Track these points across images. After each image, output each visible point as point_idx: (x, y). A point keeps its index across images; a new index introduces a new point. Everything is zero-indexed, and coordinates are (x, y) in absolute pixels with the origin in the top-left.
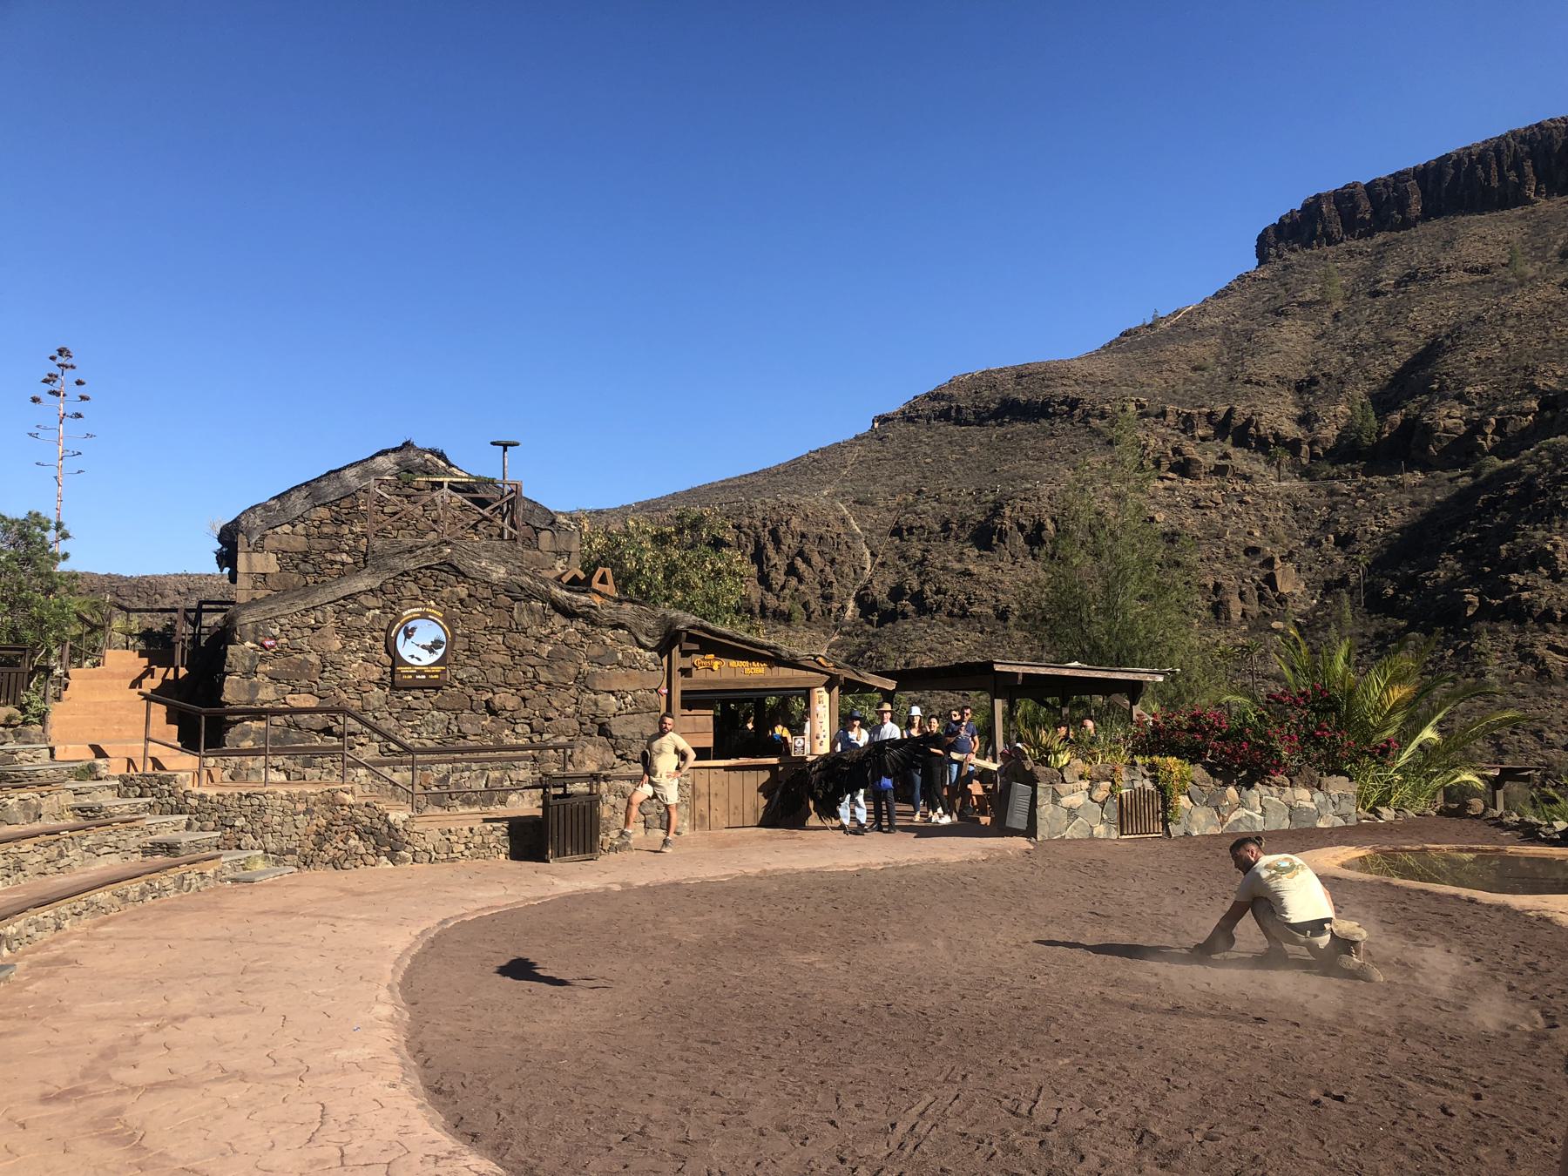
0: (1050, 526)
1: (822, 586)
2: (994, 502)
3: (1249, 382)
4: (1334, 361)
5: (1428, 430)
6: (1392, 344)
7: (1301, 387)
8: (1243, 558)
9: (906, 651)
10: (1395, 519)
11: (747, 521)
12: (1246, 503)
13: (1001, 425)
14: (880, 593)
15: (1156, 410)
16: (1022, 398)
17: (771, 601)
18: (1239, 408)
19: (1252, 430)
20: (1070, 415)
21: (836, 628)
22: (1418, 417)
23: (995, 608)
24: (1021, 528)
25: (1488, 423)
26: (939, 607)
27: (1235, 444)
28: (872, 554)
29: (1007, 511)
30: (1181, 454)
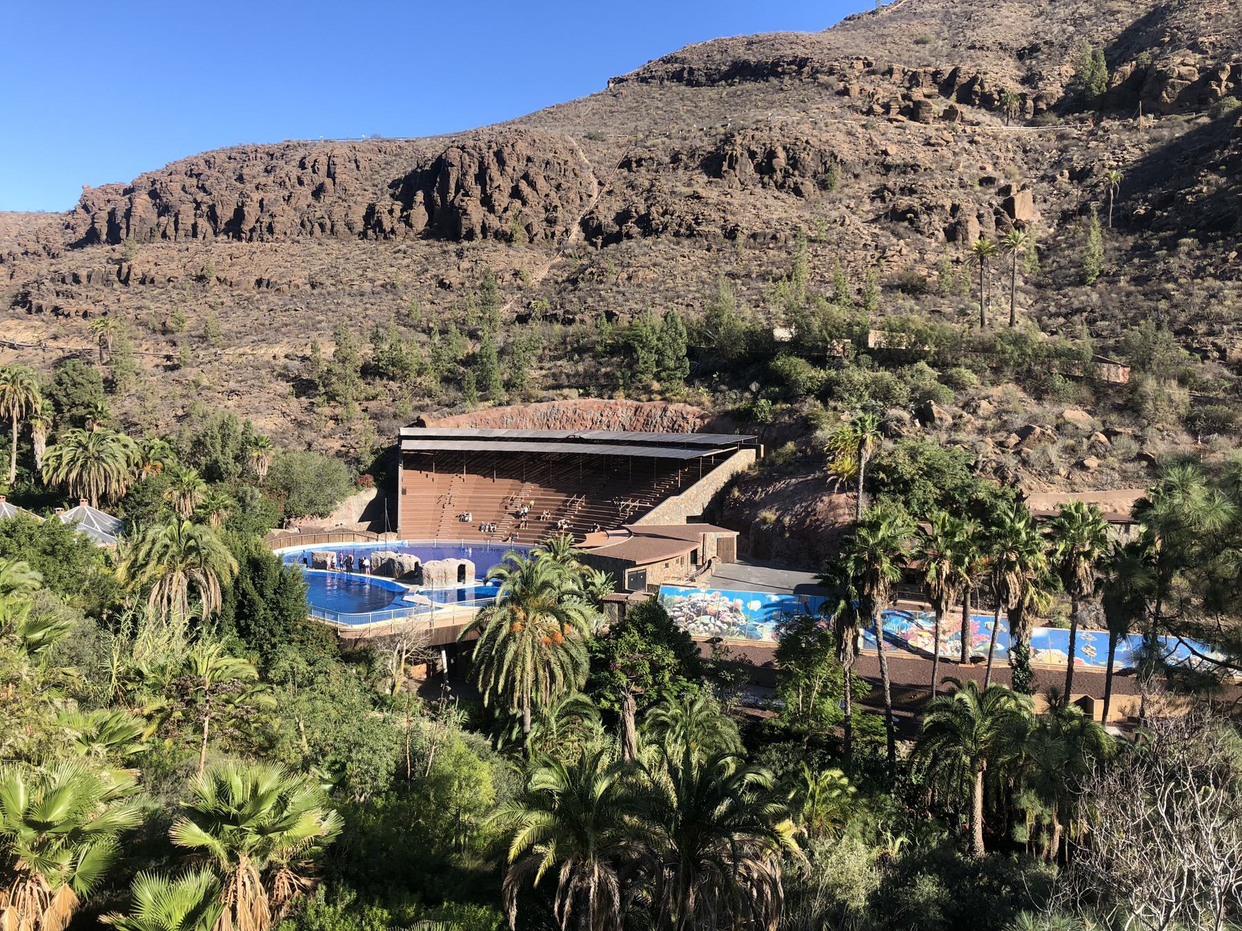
0: (782, 155)
1: (547, 210)
2: (725, 134)
3: (973, 47)
4: (1055, 31)
5: (1162, 78)
6: (1113, 13)
7: (1021, 55)
8: (978, 188)
9: (629, 265)
10: (1133, 155)
11: (471, 143)
12: (976, 143)
13: (731, 85)
14: (606, 218)
15: (884, 68)
16: (753, 60)
17: (493, 222)
18: (964, 68)
19: (977, 88)
20: (799, 73)
21: (558, 250)
22: (1152, 64)
23: (723, 228)
24: (752, 155)
25: (1223, 69)
26: (665, 227)
27: (959, 101)
28: (600, 183)
29: (738, 139)
30: (910, 100)
